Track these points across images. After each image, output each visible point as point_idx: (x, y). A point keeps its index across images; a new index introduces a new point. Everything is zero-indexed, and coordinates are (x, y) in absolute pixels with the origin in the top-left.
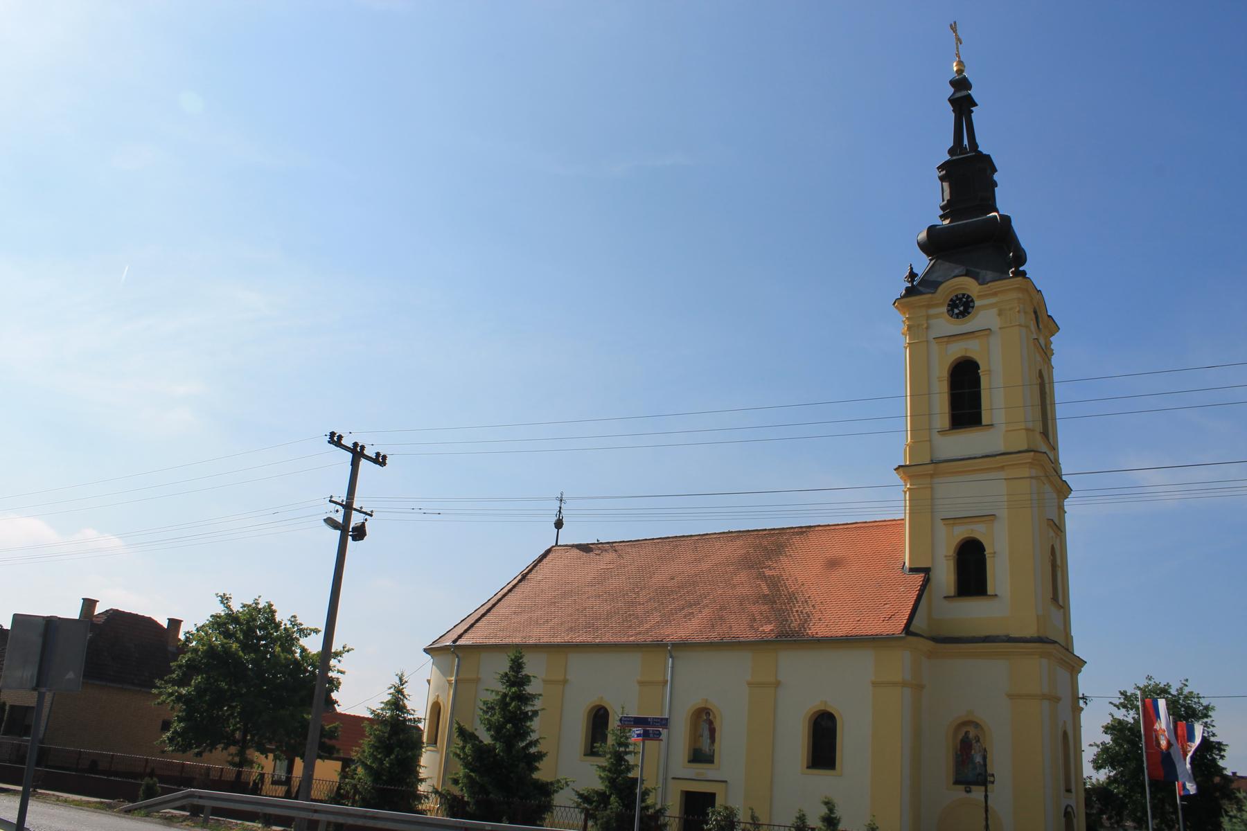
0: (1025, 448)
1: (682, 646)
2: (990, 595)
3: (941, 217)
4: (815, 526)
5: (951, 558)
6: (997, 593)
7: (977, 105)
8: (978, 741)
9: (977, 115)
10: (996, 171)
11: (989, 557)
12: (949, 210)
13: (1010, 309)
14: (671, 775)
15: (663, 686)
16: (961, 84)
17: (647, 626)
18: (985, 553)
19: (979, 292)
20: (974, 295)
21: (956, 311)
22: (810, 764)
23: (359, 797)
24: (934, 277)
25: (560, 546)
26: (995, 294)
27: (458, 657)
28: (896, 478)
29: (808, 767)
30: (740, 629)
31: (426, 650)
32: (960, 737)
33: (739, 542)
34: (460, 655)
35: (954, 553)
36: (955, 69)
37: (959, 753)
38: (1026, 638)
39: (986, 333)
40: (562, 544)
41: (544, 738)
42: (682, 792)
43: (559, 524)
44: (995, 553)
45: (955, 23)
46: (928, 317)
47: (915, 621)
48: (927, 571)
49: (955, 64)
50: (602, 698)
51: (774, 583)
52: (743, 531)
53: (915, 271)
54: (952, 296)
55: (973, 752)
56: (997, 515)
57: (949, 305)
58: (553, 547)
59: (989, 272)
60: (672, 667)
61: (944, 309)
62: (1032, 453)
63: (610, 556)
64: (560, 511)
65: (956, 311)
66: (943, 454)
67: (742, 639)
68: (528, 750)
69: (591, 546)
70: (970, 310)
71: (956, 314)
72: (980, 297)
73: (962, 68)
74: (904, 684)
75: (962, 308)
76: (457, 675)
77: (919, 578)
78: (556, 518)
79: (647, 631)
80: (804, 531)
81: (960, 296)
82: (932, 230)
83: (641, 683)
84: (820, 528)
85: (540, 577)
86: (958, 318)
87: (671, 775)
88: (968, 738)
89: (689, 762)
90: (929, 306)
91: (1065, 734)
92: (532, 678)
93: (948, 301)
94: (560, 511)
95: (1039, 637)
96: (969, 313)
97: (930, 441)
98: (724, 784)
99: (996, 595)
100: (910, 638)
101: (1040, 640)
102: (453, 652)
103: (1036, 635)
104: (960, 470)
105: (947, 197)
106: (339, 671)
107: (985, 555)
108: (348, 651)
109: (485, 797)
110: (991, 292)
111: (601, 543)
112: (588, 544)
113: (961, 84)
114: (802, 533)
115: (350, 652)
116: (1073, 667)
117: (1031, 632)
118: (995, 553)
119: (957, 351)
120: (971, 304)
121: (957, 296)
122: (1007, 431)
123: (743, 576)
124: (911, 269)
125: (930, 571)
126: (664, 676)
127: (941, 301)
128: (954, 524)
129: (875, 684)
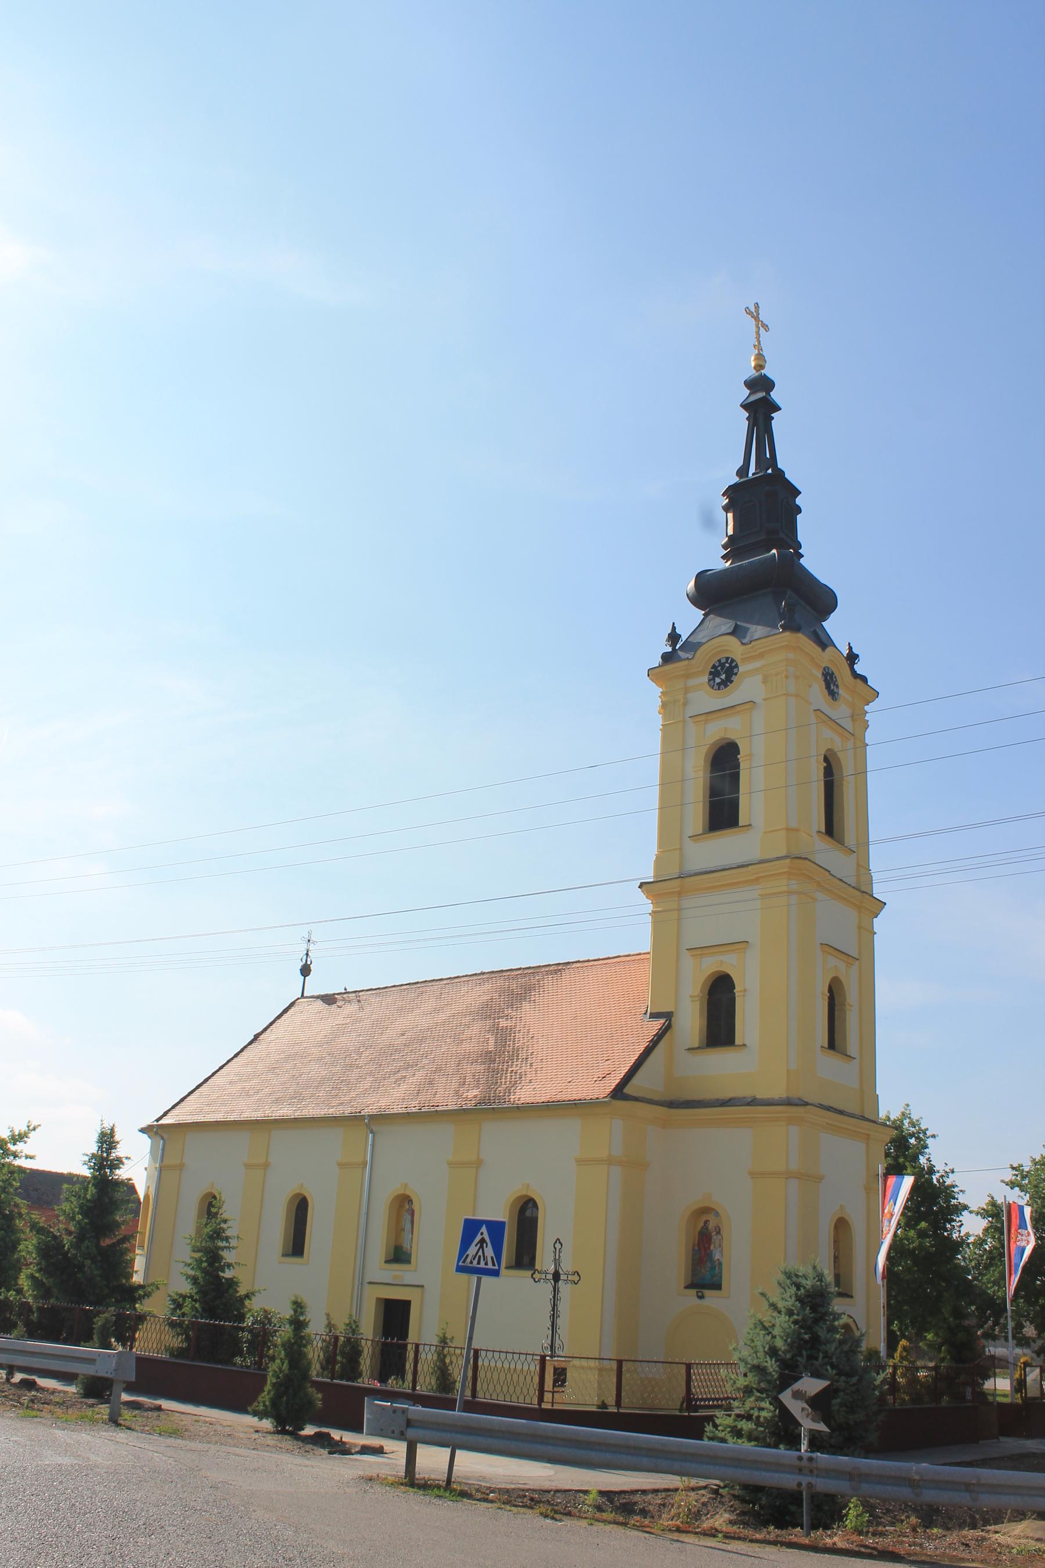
0: (783, 853)
1: (381, 1118)
2: (737, 1046)
3: (723, 557)
4: (573, 963)
5: (697, 999)
6: (745, 1043)
7: (780, 409)
8: (719, 1233)
9: (778, 422)
10: (798, 493)
11: (738, 996)
12: (734, 547)
13: (777, 675)
14: (367, 1279)
15: (363, 1168)
16: (761, 384)
17: (353, 1094)
18: (735, 991)
19: (742, 655)
20: (738, 659)
21: (718, 680)
22: (514, 1263)
23: (864, 1364)
24: (695, 639)
25: (307, 997)
26: (761, 656)
27: (162, 1138)
28: (641, 897)
29: (285, 1255)
30: (445, 1098)
31: (142, 1130)
32: (699, 1228)
33: (487, 986)
34: (165, 1136)
35: (701, 991)
36: (753, 364)
37: (696, 1248)
38: (773, 1099)
39: (748, 706)
40: (308, 995)
41: (243, 1239)
42: (378, 1300)
43: (305, 971)
44: (745, 990)
45: (757, 306)
46: (687, 690)
47: (635, 1081)
48: (668, 1016)
49: (753, 358)
50: (406, 1185)
51: (504, 1036)
52: (496, 972)
53: (678, 631)
54: (714, 661)
55: (712, 1247)
56: (750, 942)
57: (711, 673)
58: (298, 999)
59: (759, 627)
60: (373, 1146)
61: (705, 678)
62: (788, 861)
63: (351, 1008)
64: (307, 954)
65: (718, 680)
66: (693, 866)
67: (440, 1108)
68: (119, 1246)
69: (336, 996)
70: (734, 678)
71: (717, 684)
72: (747, 659)
73: (762, 363)
74: (610, 1161)
75: (723, 677)
76: (162, 1161)
77: (657, 1025)
78: (302, 964)
79: (353, 1099)
80: (558, 969)
81: (723, 661)
82: (701, 577)
83: (341, 1165)
84: (578, 965)
85: (273, 1037)
86: (719, 689)
87: (367, 1279)
88: (707, 1228)
89: (386, 1262)
90: (687, 676)
91: (841, 1225)
92: (124, 1160)
93: (709, 669)
94: (307, 954)
95: (788, 1098)
96: (732, 682)
97: (681, 849)
98: (419, 1290)
99: (744, 1045)
100: (619, 1103)
101: (788, 1102)
102: (156, 1133)
103: (784, 1096)
104: (716, 884)
105: (730, 532)
106: (27, 1157)
107: (735, 994)
108: (34, 1129)
109: (59, 1303)
110: (756, 653)
111: (349, 993)
112: (335, 994)
113: (761, 384)
114: (556, 972)
115: (37, 1130)
116: (868, 1135)
117: (779, 1092)
118: (745, 990)
119: (715, 732)
120: (735, 671)
121: (719, 661)
122: (765, 833)
123: (476, 1028)
124: (674, 628)
125: (672, 1016)
126: (364, 1158)
127: (701, 669)
128: (702, 954)
129: (580, 1162)
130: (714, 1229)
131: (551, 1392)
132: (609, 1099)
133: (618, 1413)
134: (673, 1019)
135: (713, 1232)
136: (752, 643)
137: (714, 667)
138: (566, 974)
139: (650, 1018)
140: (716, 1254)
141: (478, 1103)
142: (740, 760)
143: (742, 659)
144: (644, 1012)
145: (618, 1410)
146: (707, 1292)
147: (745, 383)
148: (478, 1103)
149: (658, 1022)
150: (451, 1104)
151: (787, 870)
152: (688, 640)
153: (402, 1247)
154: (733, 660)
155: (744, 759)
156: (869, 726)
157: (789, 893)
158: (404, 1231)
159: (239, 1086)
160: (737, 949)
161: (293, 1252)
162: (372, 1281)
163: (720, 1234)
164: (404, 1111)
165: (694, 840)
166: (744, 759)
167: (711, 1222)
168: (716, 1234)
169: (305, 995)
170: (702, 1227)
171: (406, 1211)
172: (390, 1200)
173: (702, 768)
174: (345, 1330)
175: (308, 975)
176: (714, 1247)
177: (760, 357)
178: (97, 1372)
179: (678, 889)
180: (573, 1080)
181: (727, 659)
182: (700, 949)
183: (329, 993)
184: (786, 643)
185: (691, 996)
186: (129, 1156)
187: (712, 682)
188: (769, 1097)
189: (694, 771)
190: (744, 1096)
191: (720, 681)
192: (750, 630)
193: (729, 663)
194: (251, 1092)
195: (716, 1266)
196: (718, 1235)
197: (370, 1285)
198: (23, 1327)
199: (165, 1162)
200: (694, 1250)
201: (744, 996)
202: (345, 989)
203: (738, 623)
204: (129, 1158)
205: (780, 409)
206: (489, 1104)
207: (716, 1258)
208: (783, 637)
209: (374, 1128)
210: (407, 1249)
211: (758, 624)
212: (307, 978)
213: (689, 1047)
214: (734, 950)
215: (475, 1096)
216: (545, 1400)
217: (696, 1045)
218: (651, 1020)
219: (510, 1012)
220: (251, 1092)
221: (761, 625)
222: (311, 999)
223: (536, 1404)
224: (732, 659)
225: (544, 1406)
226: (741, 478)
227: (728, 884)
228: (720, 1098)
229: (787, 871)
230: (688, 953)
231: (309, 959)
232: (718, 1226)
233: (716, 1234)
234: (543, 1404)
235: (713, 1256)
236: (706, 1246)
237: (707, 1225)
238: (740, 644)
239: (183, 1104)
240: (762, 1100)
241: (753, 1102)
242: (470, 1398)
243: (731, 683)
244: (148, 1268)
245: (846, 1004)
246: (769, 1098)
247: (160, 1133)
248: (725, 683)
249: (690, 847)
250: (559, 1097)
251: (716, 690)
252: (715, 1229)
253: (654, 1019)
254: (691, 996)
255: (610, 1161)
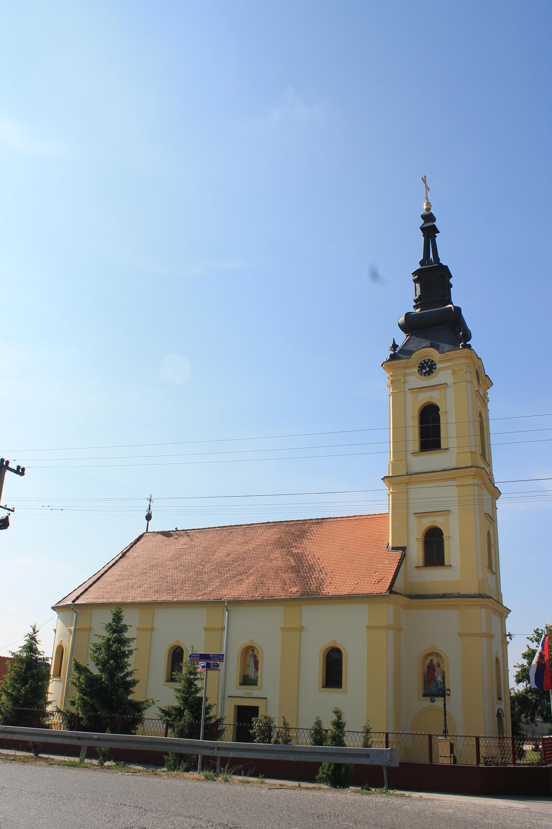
1: (236, 602)
2: (446, 566)
3: (414, 307)
5: (420, 540)
6: (451, 564)
7: (439, 232)
8: (439, 666)
9: (439, 239)
12: (420, 302)
13: (460, 370)
15: (222, 631)
16: (428, 217)
17: (210, 589)
19: (439, 358)
21: (424, 371)
25: (149, 532)
26: (450, 360)
27: (76, 612)
28: (383, 485)
31: (53, 608)
33: (275, 530)
34: (78, 611)
35: (422, 536)
36: (425, 207)
37: (426, 674)
39: (444, 386)
42: (235, 706)
43: (149, 517)
45: (425, 177)
46: (405, 375)
48: (404, 549)
49: (425, 204)
50: (252, 641)
51: (299, 558)
53: (396, 343)
55: (436, 674)
57: (419, 367)
58: (144, 533)
60: (228, 618)
61: (416, 370)
62: (475, 468)
64: (149, 508)
65: (424, 371)
67: (276, 598)
70: (433, 370)
73: (430, 207)
74: (388, 628)
75: (428, 369)
77: (399, 554)
79: (210, 592)
81: (427, 361)
84: (331, 520)
85: (135, 555)
86: (425, 376)
88: (432, 664)
89: (240, 684)
90: (405, 368)
93: (418, 365)
94: (149, 508)
99: (451, 565)
102: (73, 609)
103: (477, 593)
107: (443, 538)
111: (179, 531)
112: (169, 531)
113: (428, 217)
114: (318, 523)
116: (503, 614)
117: (474, 590)
119: (424, 398)
120: (434, 367)
121: (424, 361)
122: (457, 453)
123: (277, 553)
124: (394, 342)
127: (414, 364)
128: (422, 516)
130: (436, 664)
131: (449, 757)
132: (388, 594)
133: (515, 768)
134: (406, 550)
135: (436, 666)
136: (446, 353)
137: (421, 363)
138: (325, 525)
139: (392, 550)
140: (438, 678)
141: (302, 595)
142: (440, 414)
143: (438, 361)
144: (386, 547)
145: (515, 766)
146: (436, 699)
147: (422, 216)
148: (302, 595)
149: (398, 552)
150: (283, 595)
151: (473, 473)
152: (403, 348)
153: (249, 676)
154: (432, 361)
155: (442, 414)
156: (489, 401)
157: (474, 485)
158: (249, 667)
159: (125, 583)
160: (444, 514)
161: (171, 680)
162: (231, 695)
163: (440, 667)
164: (252, 599)
165: (414, 455)
166: (442, 414)
167: (434, 661)
168: (438, 667)
169: (148, 531)
170: (429, 663)
171: (250, 656)
172: (170, 648)
173: (417, 417)
174: (314, 726)
175: (150, 520)
176: (437, 674)
177: (428, 204)
178: (372, 762)
179: (407, 481)
180: (359, 583)
181: (429, 360)
182: (422, 514)
183: (165, 530)
184: (466, 354)
185: (416, 539)
186: (131, 625)
187: (420, 371)
188: (468, 593)
189: (412, 418)
190: (452, 593)
191: (425, 371)
192: (441, 346)
193: (430, 363)
194: (135, 586)
195: (438, 684)
196: (439, 667)
197: (230, 698)
198: (109, 730)
199: (78, 626)
200: (425, 676)
201: (449, 539)
202: (176, 529)
203: (432, 342)
204: (131, 626)
205: (439, 232)
206: (309, 596)
207: (438, 680)
208: (457, 353)
209: (229, 609)
210: (252, 677)
211: (445, 343)
212: (149, 521)
213: (416, 566)
214: (442, 515)
215: (297, 591)
216: (481, 762)
217: (421, 565)
218: (393, 551)
219: (297, 544)
220: (135, 586)
221: (447, 344)
222: (154, 534)
223: (476, 764)
224: (432, 360)
225: (481, 766)
226: (422, 266)
227: (434, 480)
228: (438, 594)
229: (473, 474)
230: (414, 516)
231: (150, 511)
232: (438, 663)
233: (438, 667)
234: (480, 764)
235: (437, 678)
236: (432, 673)
237: (432, 662)
238: (438, 353)
239: (87, 592)
240: (463, 595)
241: (460, 596)
242: (429, 763)
243: (432, 373)
244: (67, 689)
245: (491, 545)
246: (468, 594)
247: (75, 609)
248: (429, 373)
249: (411, 458)
250: (354, 592)
251: (423, 376)
252: (437, 664)
253: (395, 551)
254: (416, 539)
255: (388, 628)
